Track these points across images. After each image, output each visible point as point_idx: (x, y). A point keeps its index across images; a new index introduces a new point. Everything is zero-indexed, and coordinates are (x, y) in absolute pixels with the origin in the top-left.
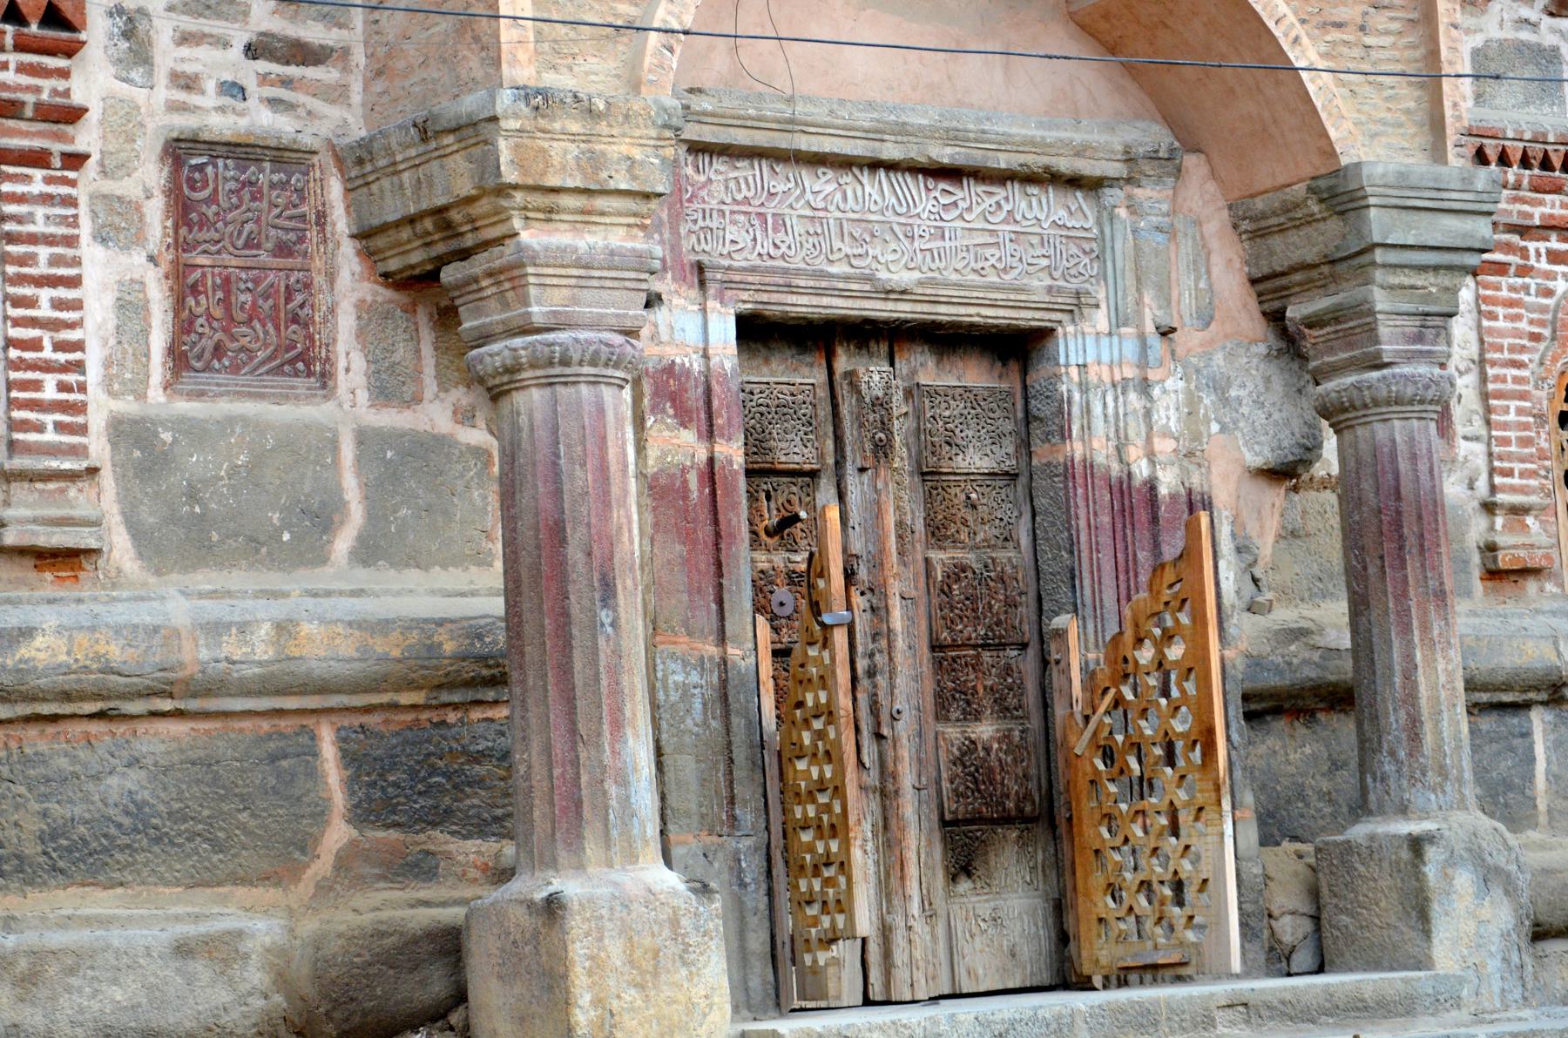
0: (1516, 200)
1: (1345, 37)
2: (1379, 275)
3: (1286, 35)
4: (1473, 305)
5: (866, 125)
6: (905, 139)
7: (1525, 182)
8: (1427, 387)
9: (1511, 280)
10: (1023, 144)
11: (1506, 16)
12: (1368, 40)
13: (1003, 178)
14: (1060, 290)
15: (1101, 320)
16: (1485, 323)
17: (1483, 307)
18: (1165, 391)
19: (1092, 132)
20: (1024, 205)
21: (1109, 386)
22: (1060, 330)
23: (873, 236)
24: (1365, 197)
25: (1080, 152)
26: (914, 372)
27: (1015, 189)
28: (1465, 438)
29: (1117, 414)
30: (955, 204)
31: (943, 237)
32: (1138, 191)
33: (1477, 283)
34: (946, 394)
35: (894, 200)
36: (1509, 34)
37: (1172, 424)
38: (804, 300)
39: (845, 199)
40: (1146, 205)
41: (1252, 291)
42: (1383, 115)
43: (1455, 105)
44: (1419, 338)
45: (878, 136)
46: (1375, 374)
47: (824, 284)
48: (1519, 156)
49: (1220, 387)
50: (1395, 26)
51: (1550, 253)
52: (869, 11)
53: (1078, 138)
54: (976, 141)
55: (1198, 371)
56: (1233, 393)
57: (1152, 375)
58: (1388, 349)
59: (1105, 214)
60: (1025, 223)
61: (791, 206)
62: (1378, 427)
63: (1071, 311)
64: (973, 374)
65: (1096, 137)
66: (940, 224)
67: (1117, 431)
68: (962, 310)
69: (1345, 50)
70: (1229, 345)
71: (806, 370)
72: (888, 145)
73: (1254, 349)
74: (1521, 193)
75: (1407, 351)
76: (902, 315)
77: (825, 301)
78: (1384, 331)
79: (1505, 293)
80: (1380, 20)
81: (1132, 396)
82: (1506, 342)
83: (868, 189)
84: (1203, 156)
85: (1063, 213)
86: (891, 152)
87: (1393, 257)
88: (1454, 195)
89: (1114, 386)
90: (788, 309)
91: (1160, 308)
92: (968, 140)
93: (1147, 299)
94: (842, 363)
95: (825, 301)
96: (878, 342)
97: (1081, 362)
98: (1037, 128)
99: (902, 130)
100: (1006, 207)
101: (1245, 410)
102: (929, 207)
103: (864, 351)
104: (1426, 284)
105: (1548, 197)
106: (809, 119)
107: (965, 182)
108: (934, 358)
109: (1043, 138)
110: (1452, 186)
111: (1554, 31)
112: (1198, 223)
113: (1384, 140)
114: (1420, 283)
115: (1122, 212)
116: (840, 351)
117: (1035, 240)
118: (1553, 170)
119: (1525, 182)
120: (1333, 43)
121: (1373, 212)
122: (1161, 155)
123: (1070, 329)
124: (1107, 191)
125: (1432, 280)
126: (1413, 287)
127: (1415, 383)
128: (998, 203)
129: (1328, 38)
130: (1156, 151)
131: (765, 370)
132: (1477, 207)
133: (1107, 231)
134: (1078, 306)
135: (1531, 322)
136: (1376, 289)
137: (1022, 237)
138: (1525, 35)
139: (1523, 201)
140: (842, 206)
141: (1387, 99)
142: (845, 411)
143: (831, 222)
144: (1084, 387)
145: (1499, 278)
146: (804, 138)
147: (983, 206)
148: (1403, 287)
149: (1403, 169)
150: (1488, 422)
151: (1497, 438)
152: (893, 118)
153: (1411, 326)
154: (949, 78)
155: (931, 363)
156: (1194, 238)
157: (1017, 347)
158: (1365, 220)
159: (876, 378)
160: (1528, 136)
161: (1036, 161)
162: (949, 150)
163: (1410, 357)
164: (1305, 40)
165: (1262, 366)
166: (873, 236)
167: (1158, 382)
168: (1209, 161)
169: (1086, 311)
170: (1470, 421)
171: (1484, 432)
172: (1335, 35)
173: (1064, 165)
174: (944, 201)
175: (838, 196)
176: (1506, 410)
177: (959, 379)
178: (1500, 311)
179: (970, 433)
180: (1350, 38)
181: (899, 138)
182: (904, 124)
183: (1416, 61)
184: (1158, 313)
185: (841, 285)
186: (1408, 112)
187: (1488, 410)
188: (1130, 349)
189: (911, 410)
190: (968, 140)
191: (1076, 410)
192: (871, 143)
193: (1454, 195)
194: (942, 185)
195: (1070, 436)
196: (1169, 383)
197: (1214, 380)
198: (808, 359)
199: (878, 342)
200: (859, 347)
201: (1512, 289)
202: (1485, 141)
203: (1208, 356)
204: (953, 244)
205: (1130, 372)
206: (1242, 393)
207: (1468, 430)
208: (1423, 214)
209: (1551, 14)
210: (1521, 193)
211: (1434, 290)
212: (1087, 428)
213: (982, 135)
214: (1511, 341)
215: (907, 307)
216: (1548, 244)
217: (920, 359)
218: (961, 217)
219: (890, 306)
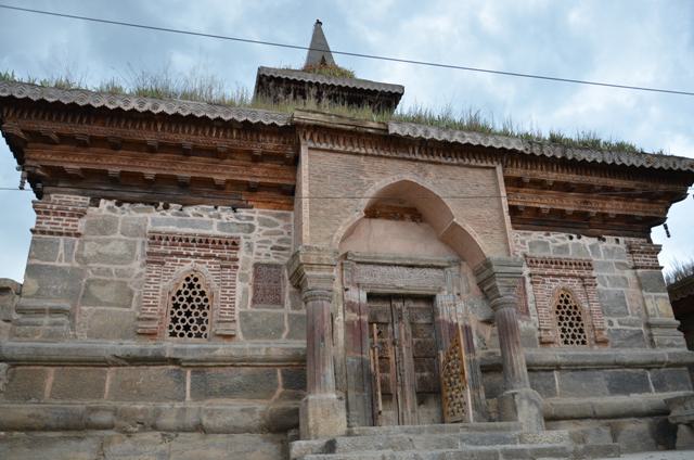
13: (423, 267)
15: (446, 293)
49: (472, 305)
58: (501, 294)
64: (422, 305)
80: (495, 232)
86: (397, 262)
99: (400, 258)
134: (440, 290)
173: (435, 264)
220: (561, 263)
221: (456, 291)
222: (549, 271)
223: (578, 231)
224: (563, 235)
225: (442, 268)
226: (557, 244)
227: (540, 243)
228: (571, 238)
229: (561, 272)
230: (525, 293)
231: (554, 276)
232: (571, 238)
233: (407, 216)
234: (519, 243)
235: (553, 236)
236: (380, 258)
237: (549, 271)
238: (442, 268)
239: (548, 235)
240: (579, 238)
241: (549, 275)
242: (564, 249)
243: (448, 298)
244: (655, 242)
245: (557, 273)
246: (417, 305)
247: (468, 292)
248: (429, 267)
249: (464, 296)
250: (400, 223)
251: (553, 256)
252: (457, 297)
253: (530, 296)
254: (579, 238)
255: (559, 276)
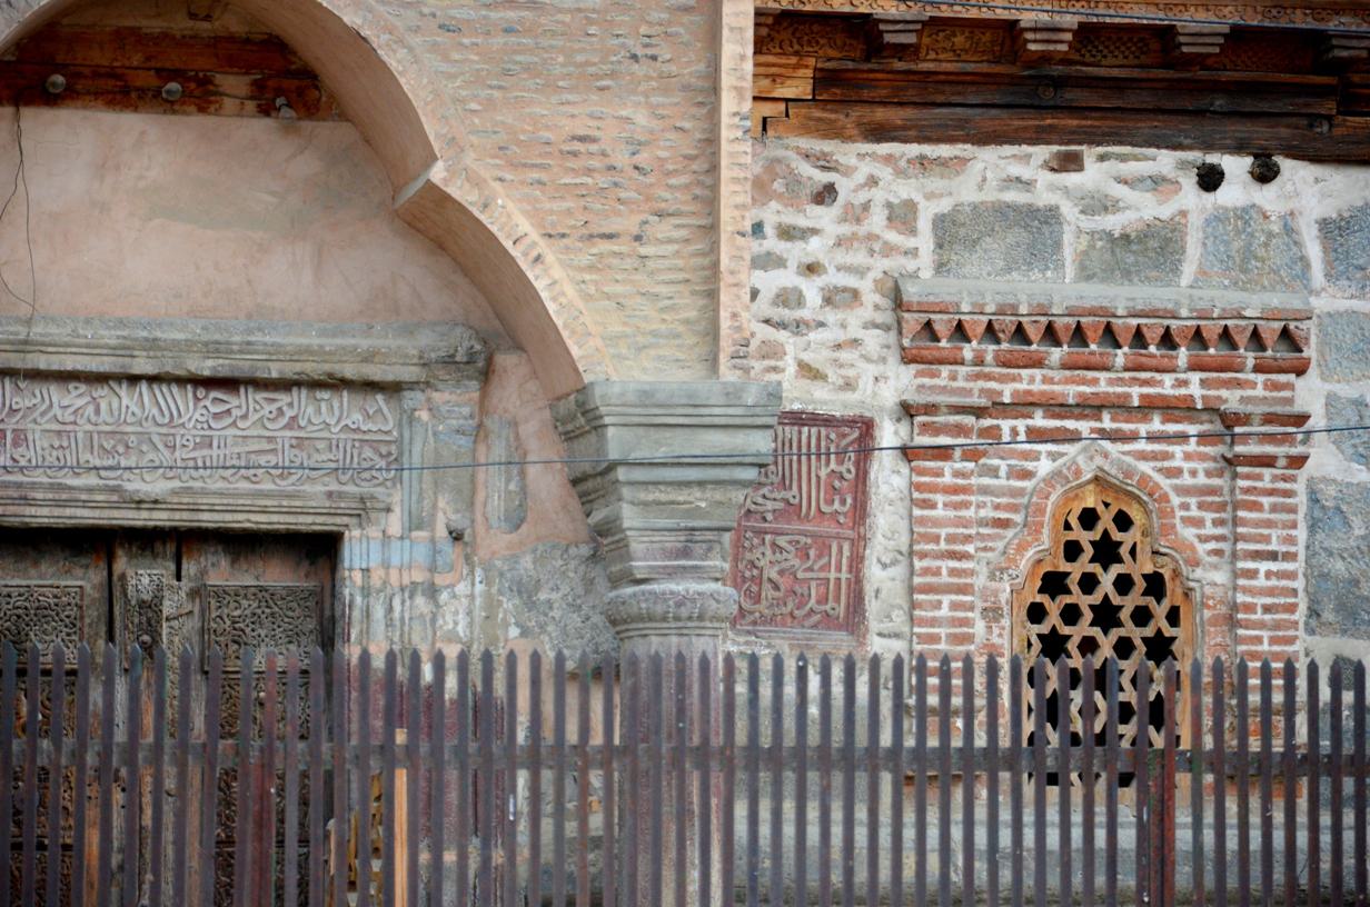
0: (978, 376)
1: (616, 248)
2: (626, 492)
3: (525, 254)
4: (906, 492)
5: (113, 342)
6: (159, 354)
7: (989, 358)
8: (679, 605)
9: (958, 465)
10: (296, 353)
11: (989, 175)
12: (643, 251)
13: (284, 385)
14: (341, 495)
15: (394, 523)
16: (917, 512)
17: (916, 495)
18: (454, 596)
19: (386, 337)
20: (310, 410)
21: (397, 590)
22: (347, 533)
23: (128, 447)
24: (601, 417)
25: (368, 357)
26: (203, 573)
27: (300, 397)
28: (880, 635)
29: (402, 619)
30: (229, 411)
31: (211, 445)
32: (436, 395)
33: (912, 470)
34: (238, 593)
35: (155, 411)
36: (990, 195)
37: (460, 629)
38: (45, 511)
39: (97, 411)
40: (444, 409)
41: (574, 492)
42: (654, 327)
43: (734, 316)
44: (685, 553)
45: (128, 352)
46: (630, 590)
47: (64, 496)
48: (981, 329)
49: (526, 591)
50: (683, 233)
51: (1030, 431)
52: (157, 222)
53: (364, 343)
54: (241, 352)
55: (502, 575)
56: (543, 596)
57: (439, 580)
58: (640, 566)
59: (405, 417)
60: (311, 428)
61: (35, 421)
62: (655, 640)
63: (359, 515)
64: (277, 575)
65: (387, 342)
66: (207, 433)
67: (402, 635)
68: (228, 517)
69: (615, 262)
70: (541, 548)
71: (79, 572)
72: (141, 361)
73: (573, 551)
74: (987, 370)
75: (665, 567)
76: (159, 523)
77: (68, 512)
78: (637, 547)
79: (948, 479)
80: (664, 229)
81: (420, 600)
82: (943, 532)
83: (125, 401)
84: (524, 355)
85: (357, 416)
86: (142, 365)
87: (639, 474)
88: (717, 411)
89: (402, 590)
90: (27, 520)
91: (457, 511)
92: (232, 352)
93: (441, 504)
94: (121, 564)
95: (68, 512)
96: (164, 544)
97: (364, 566)
98: (319, 336)
99: (152, 345)
100: (289, 413)
101: (556, 613)
102: (197, 416)
103: (148, 553)
104: (691, 499)
105: (1025, 373)
106: (47, 340)
107: (242, 390)
108: (229, 559)
109: (321, 346)
110: (712, 402)
111: (1052, 188)
112: (514, 424)
113: (653, 352)
114: (681, 499)
115: (424, 415)
116: (120, 552)
117: (321, 445)
118: (1029, 343)
119: (989, 358)
120: (601, 255)
121: (611, 431)
122: (458, 359)
123: (356, 533)
124: (407, 394)
125: (698, 495)
126: (672, 503)
127: (665, 600)
128: (280, 409)
129: (595, 251)
130: (453, 356)
131: (33, 572)
132: (748, 421)
133: (406, 434)
134: (363, 510)
135: (997, 507)
136: (625, 505)
137: (306, 442)
138: (1013, 196)
139: (988, 377)
140: (93, 419)
141: (662, 310)
142: (117, 610)
143: (80, 435)
144: (366, 591)
145: (940, 464)
146: (43, 358)
147: (262, 413)
148: (659, 503)
149: (647, 387)
150: (912, 620)
151: (919, 636)
152: (145, 334)
153: (673, 541)
154: (249, 281)
155: (224, 563)
156: (507, 439)
157: (320, 549)
158: (602, 438)
159: (146, 580)
160: (991, 308)
161: (313, 369)
162: (210, 363)
163: (671, 573)
164: (550, 258)
165: (583, 567)
166: (128, 447)
167: (447, 587)
168: (530, 360)
169: (373, 515)
170: (889, 617)
171: (906, 629)
172: (604, 246)
173: (349, 371)
174: (214, 409)
175: (90, 409)
176: (938, 605)
177: (257, 578)
178: (940, 498)
179: (263, 633)
180: (624, 249)
181: (152, 353)
182: (155, 340)
183: (704, 269)
184: (453, 517)
185: (84, 497)
186: (687, 322)
187: (913, 605)
188: (421, 554)
189: (197, 610)
190: (232, 352)
191: (356, 614)
192: (120, 359)
193: (717, 411)
194: (214, 394)
195: (349, 640)
196: (462, 588)
197: (520, 583)
198: (84, 561)
199: (164, 544)
200: (143, 549)
201: (957, 474)
202: (933, 316)
203: (514, 559)
204: (221, 453)
205: (419, 576)
206: (554, 596)
207: (886, 626)
208: (679, 431)
209: (1053, 170)
210: (987, 370)
211: (703, 505)
212: (366, 632)
213: (247, 347)
214: (952, 530)
215: (164, 515)
216: (1030, 422)
217: (212, 559)
218: (234, 424)
219: (145, 514)
220: (1167, 340)
221: (446, 514)
222: (1030, 381)
223: (1260, 132)
224: (1164, 161)
225: (392, 389)
226: (1114, 223)
227: (1007, 215)
228: (1210, 179)
229: (1103, 384)
230: (860, 512)
231: (1057, 408)
232: (1210, 179)
233: (233, 84)
234: (877, 221)
235: (1099, 170)
236: (42, 346)
237: (1030, 381)
238: (392, 389)
239: (1070, 163)
240: (1265, 174)
241: (1023, 406)
242: (1154, 247)
243: (397, 555)
244: (581, 546)
245: (1072, 392)
246: (245, 578)
247: (516, 521)
248: (315, 385)
249: (494, 541)
250: (190, 126)
251: (1096, 294)
252: (450, 552)
253: (887, 522)
254: (1265, 174)
255: (1090, 408)
